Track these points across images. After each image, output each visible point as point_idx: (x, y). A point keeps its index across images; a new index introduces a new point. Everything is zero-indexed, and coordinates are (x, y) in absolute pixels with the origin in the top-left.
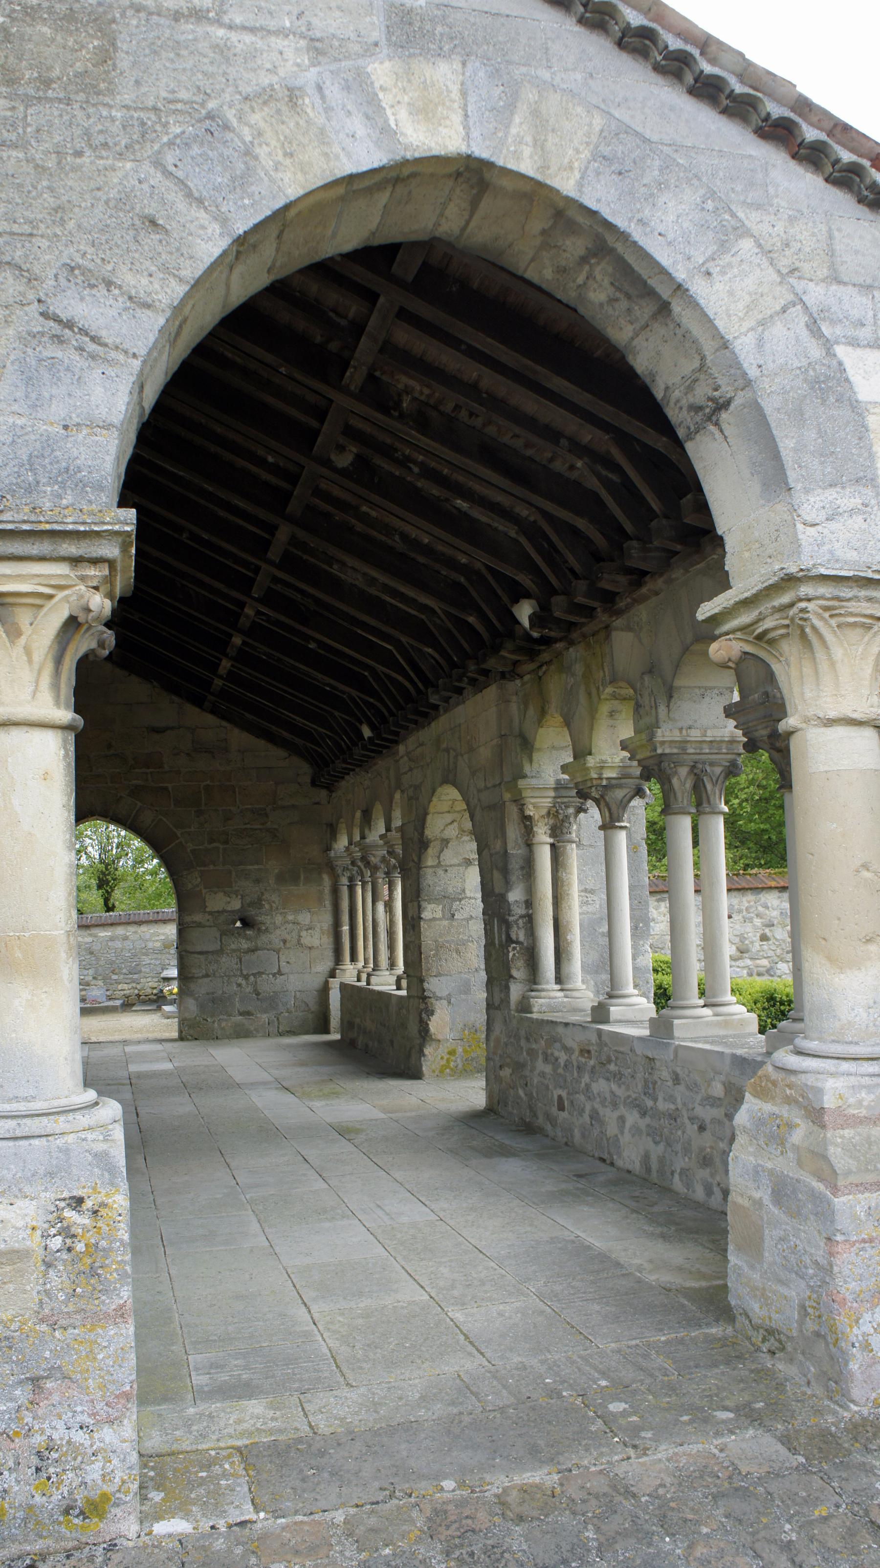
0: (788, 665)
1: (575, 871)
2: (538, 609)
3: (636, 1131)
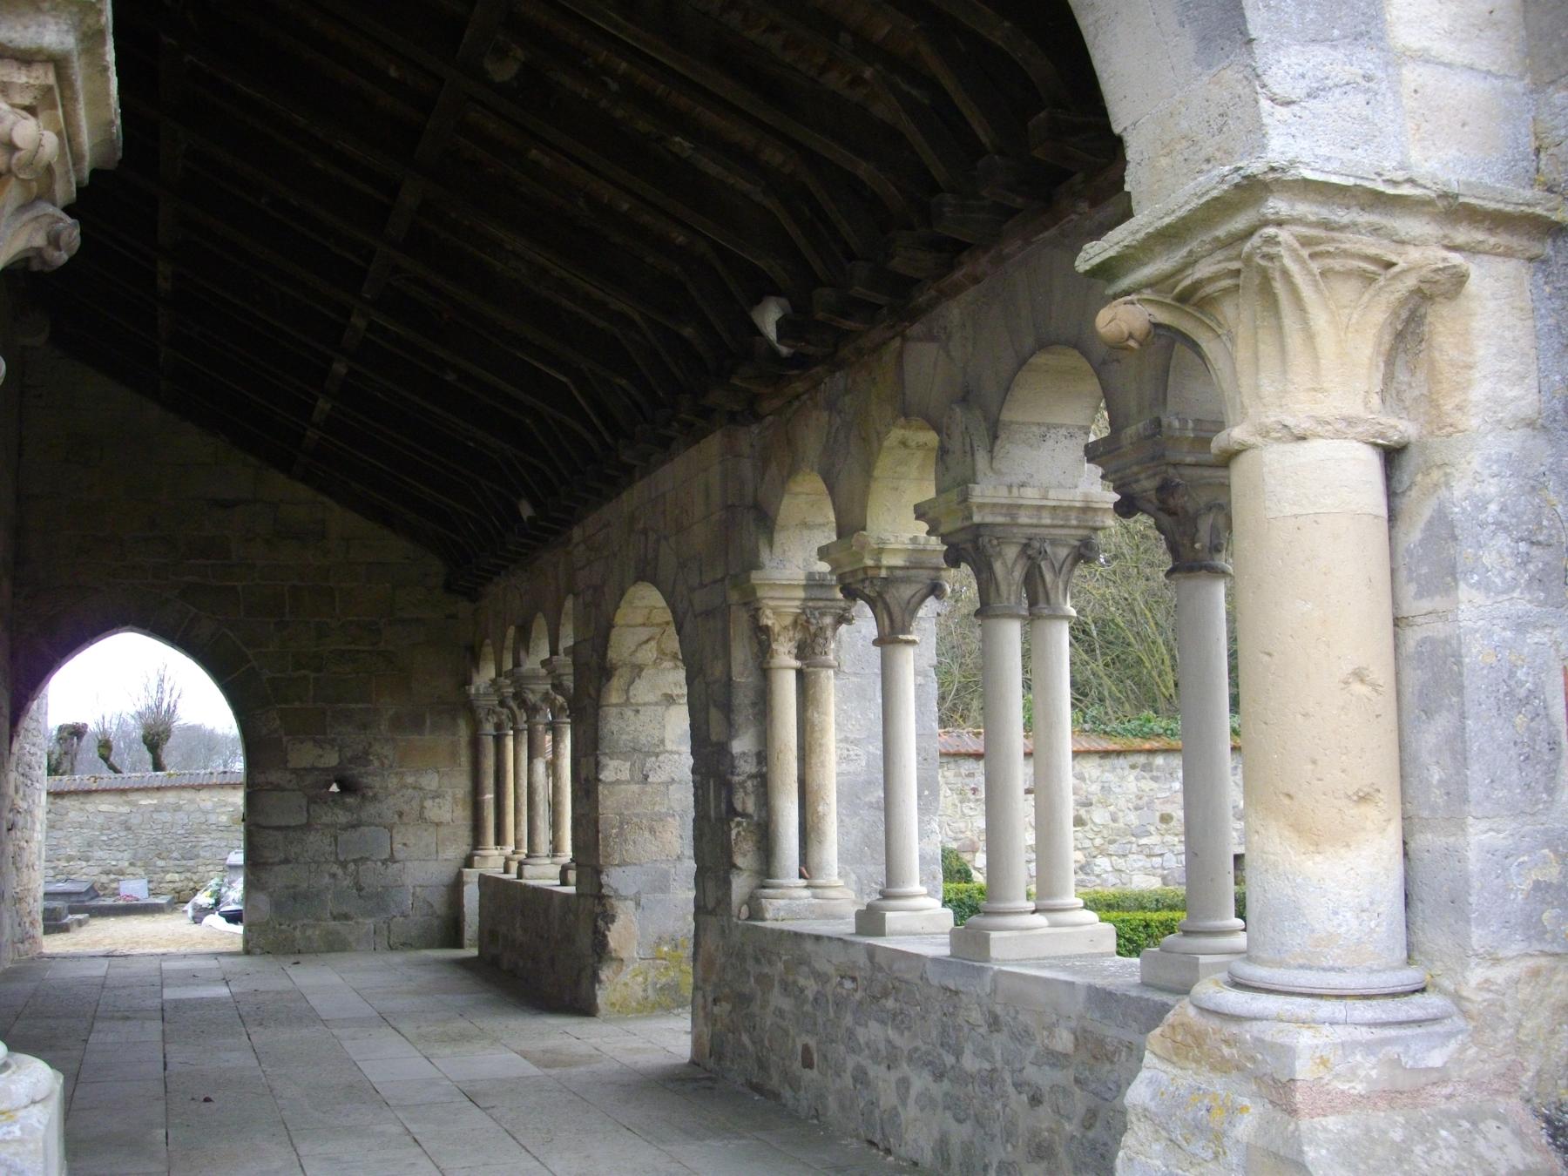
0: (1232, 340)
1: (832, 709)
2: (789, 310)
3: (926, 1102)
